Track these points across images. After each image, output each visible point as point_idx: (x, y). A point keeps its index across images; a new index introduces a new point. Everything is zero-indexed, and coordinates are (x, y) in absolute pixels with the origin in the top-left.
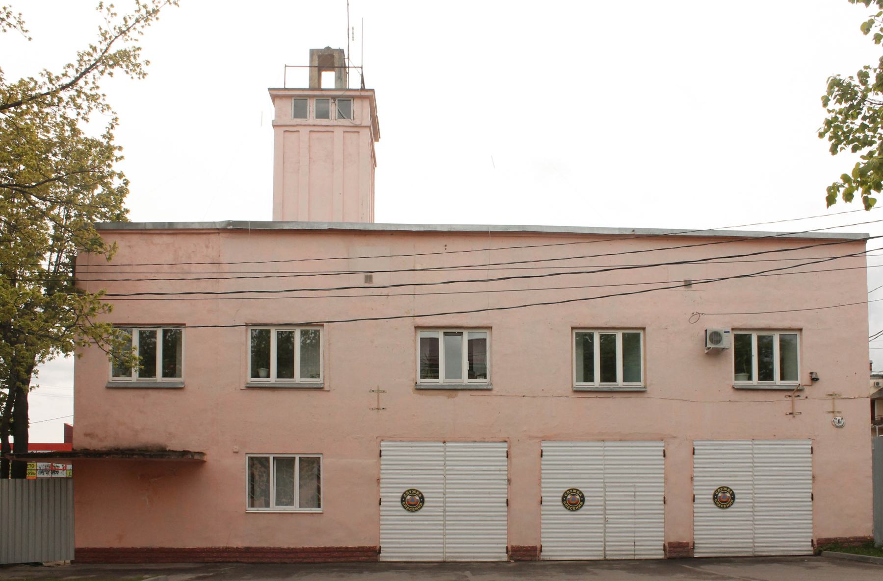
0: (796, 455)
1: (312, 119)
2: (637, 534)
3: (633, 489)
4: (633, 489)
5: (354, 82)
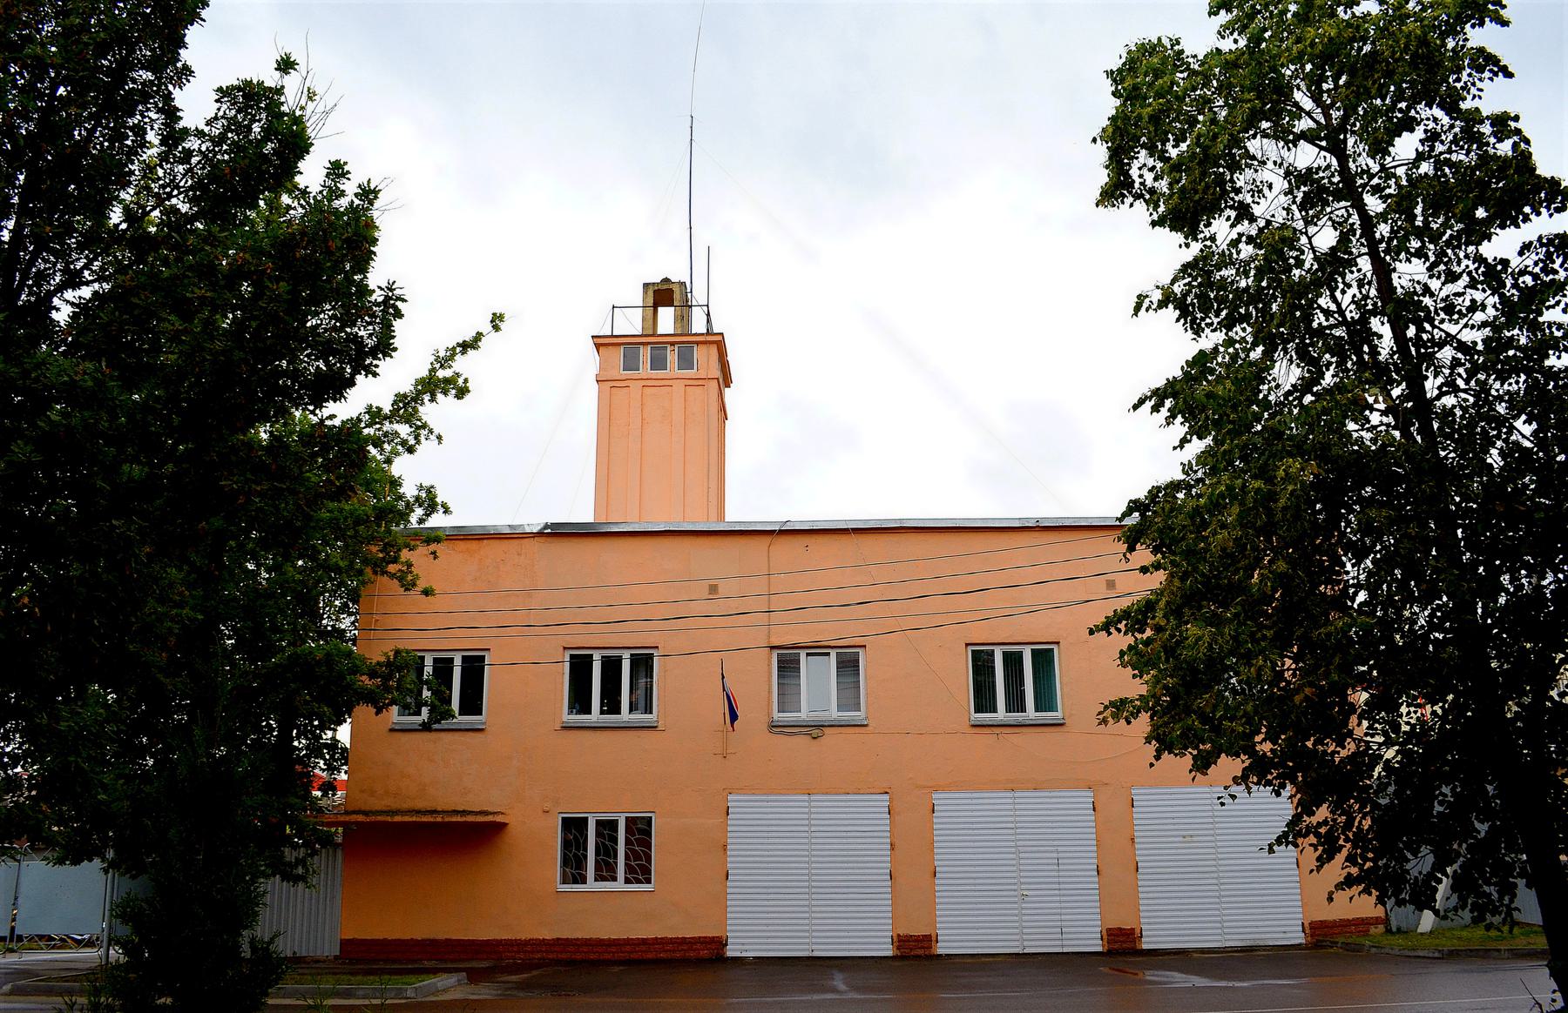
0: (992, 801)
1: (645, 370)
3: (1055, 855)
4: (1055, 855)
5: (698, 326)
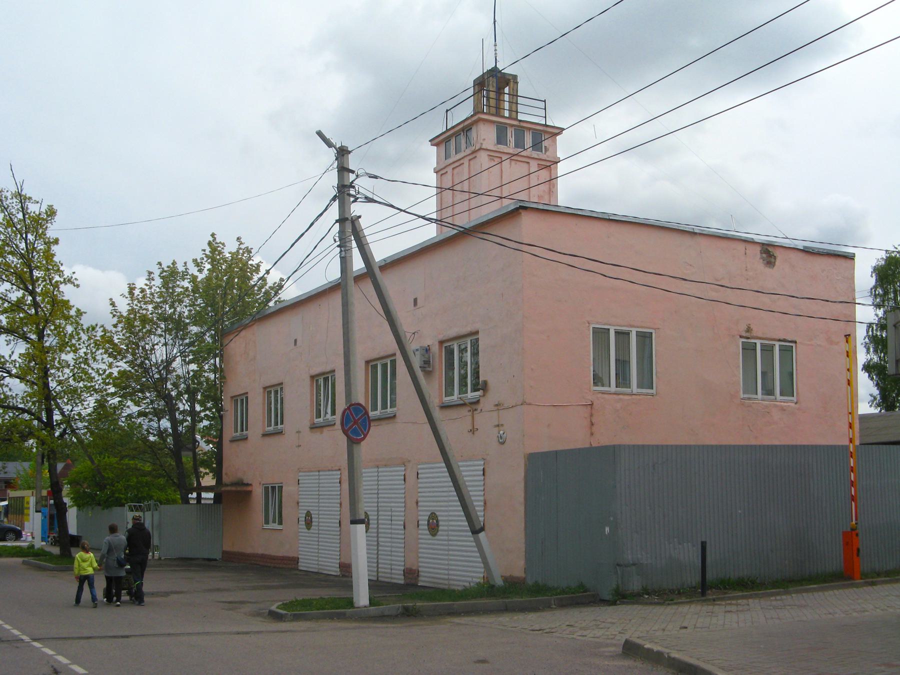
2: (451, 572)
